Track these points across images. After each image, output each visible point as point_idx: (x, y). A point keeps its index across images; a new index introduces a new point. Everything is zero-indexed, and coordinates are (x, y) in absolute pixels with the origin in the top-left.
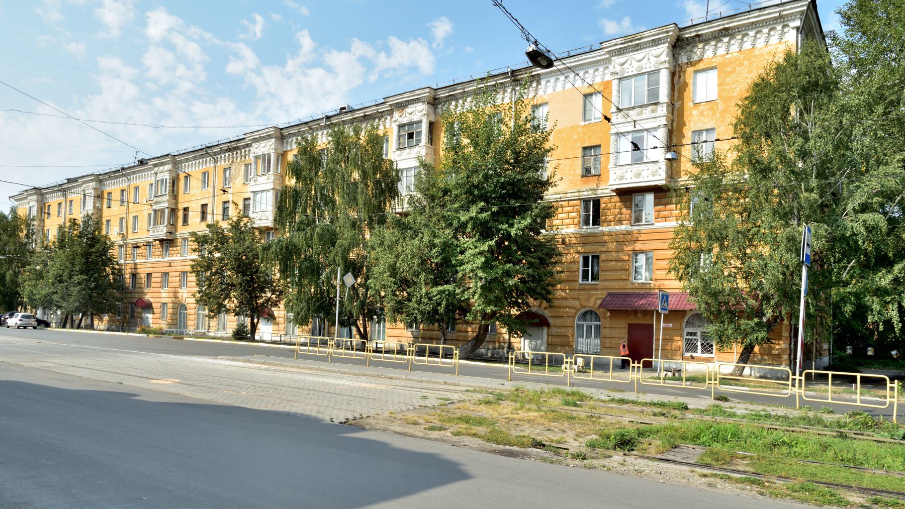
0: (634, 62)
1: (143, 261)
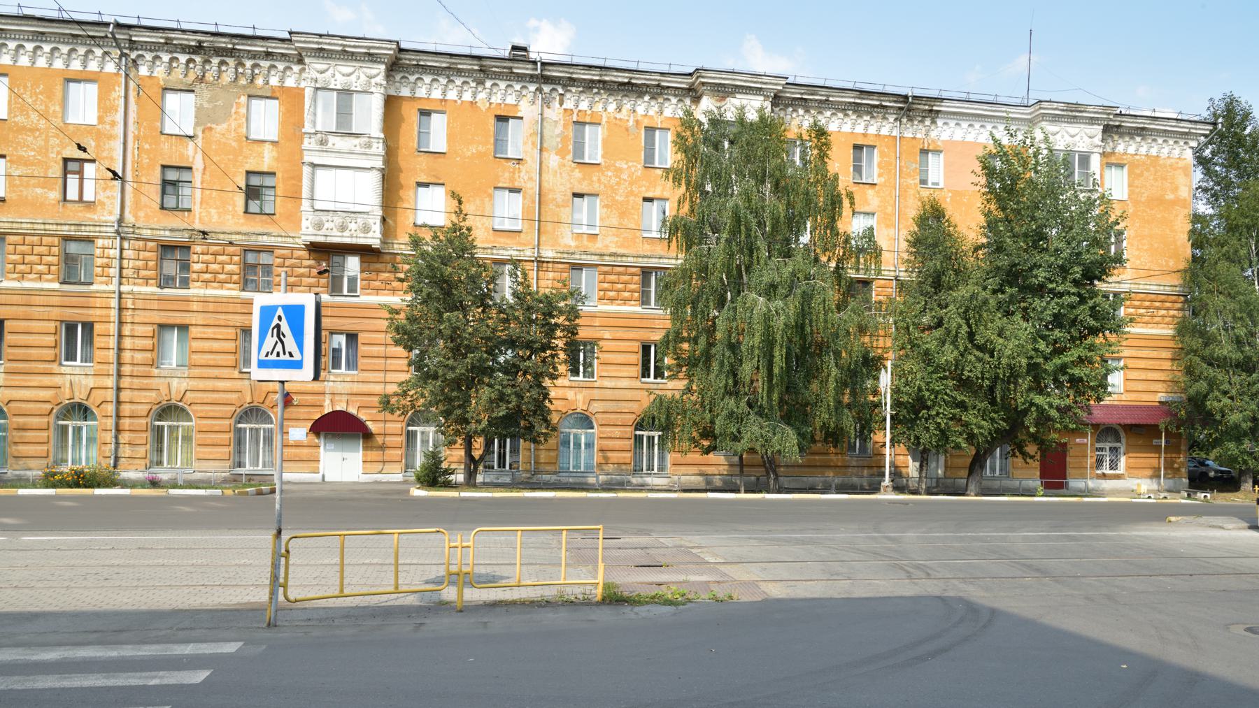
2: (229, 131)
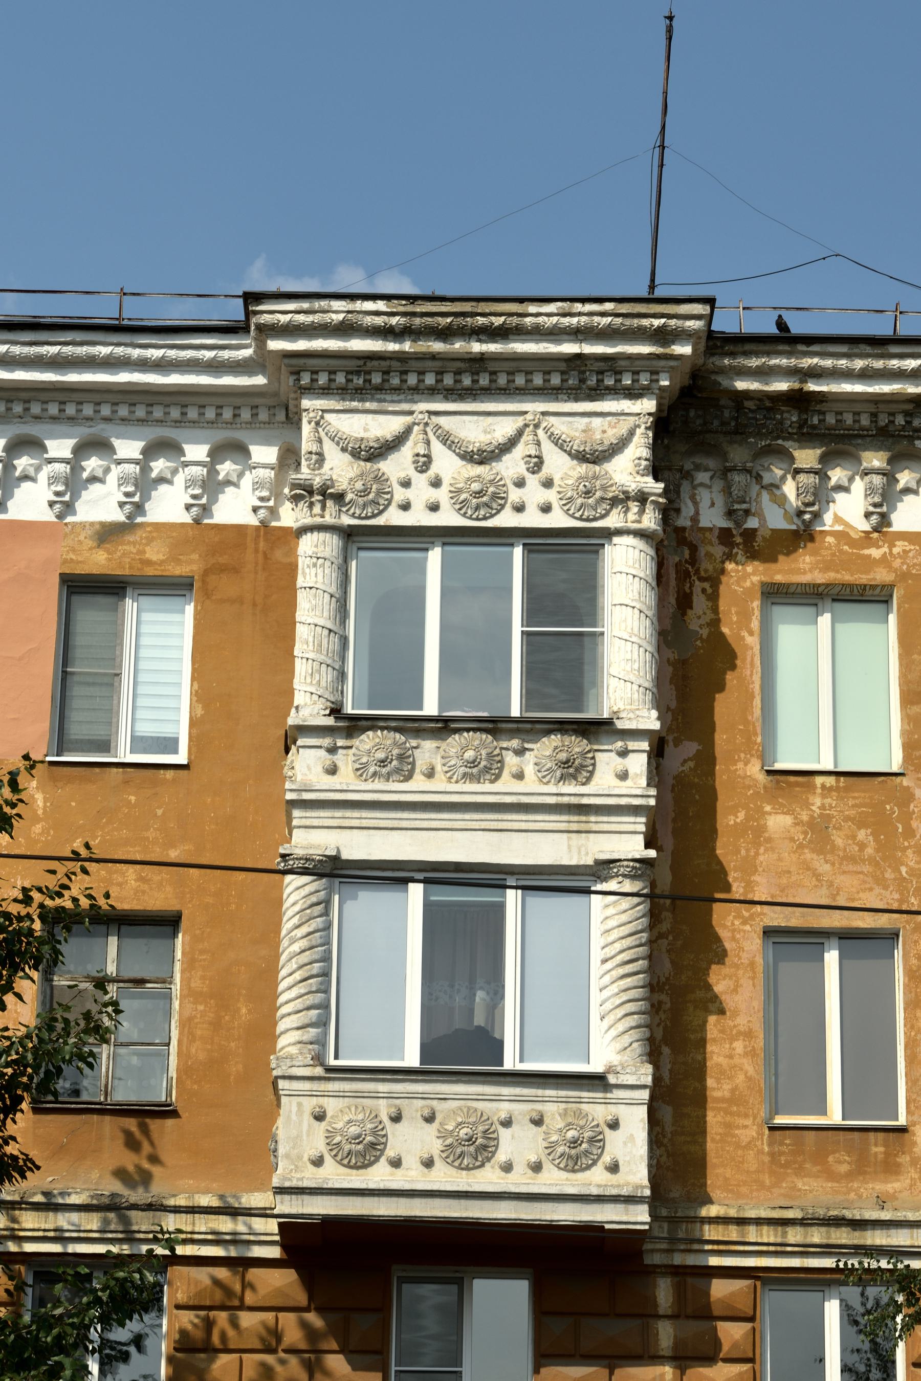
0: (431, 461)
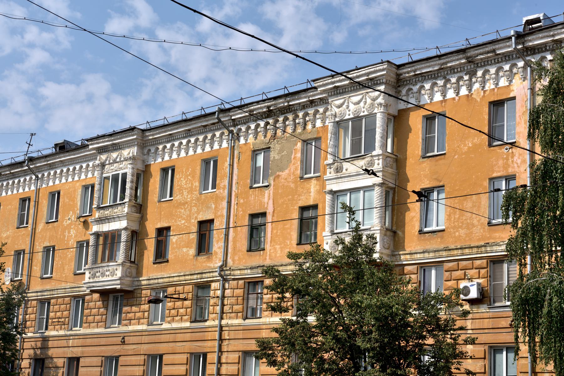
1: (62, 333)
2: (289, 175)
